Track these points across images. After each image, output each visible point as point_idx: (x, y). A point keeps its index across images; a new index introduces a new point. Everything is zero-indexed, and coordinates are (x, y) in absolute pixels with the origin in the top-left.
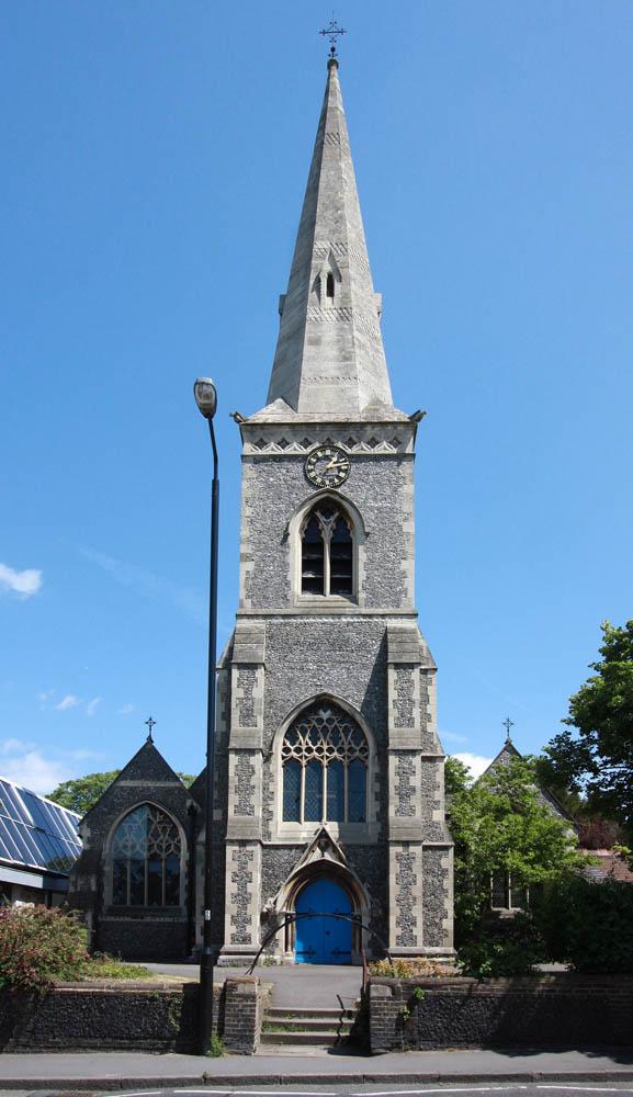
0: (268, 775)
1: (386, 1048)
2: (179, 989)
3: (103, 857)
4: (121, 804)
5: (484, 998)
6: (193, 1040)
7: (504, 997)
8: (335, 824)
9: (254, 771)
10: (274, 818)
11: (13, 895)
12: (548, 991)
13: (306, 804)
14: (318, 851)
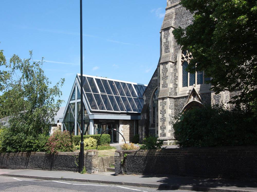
0: (176, 70)
1: (118, 173)
2: (78, 154)
3: (149, 107)
4: (154, 86)
5: (142, 157)
6: (79, 169)
7: (147, 156)
8: (199, 86)
9: (167, 70)
10: (178, 87)
11: (120, 123)
12: (159, 154)
13: (190, 79)
14: (192, 97)
